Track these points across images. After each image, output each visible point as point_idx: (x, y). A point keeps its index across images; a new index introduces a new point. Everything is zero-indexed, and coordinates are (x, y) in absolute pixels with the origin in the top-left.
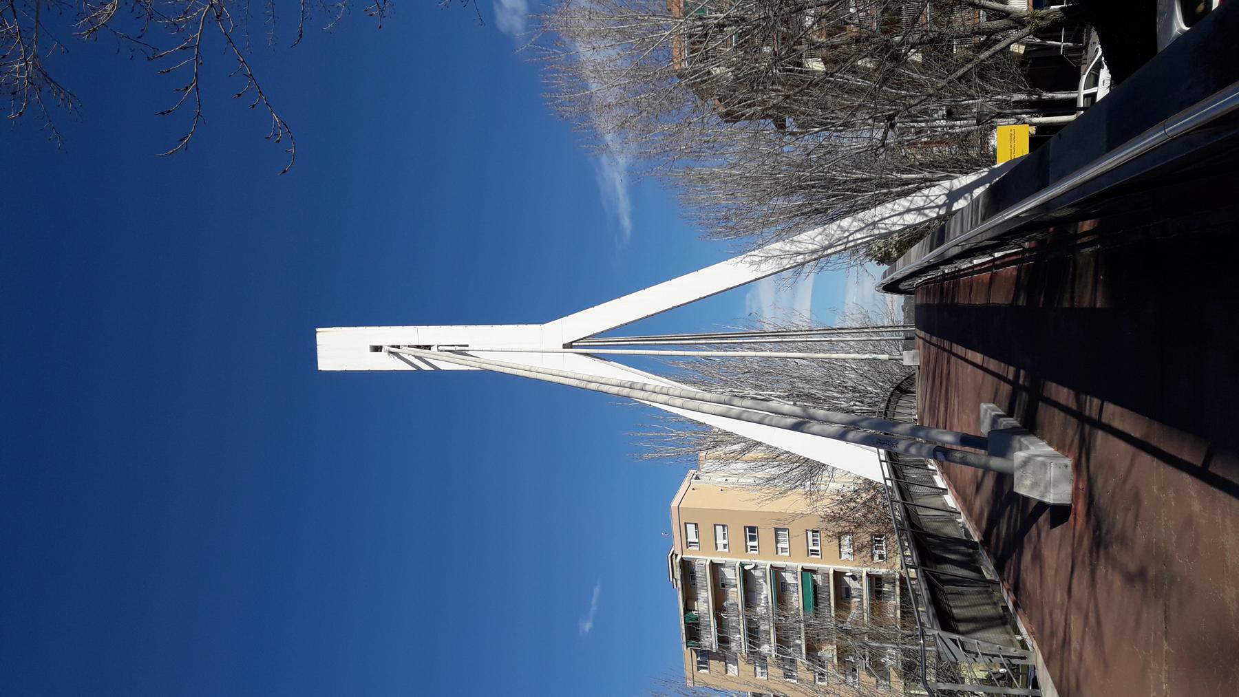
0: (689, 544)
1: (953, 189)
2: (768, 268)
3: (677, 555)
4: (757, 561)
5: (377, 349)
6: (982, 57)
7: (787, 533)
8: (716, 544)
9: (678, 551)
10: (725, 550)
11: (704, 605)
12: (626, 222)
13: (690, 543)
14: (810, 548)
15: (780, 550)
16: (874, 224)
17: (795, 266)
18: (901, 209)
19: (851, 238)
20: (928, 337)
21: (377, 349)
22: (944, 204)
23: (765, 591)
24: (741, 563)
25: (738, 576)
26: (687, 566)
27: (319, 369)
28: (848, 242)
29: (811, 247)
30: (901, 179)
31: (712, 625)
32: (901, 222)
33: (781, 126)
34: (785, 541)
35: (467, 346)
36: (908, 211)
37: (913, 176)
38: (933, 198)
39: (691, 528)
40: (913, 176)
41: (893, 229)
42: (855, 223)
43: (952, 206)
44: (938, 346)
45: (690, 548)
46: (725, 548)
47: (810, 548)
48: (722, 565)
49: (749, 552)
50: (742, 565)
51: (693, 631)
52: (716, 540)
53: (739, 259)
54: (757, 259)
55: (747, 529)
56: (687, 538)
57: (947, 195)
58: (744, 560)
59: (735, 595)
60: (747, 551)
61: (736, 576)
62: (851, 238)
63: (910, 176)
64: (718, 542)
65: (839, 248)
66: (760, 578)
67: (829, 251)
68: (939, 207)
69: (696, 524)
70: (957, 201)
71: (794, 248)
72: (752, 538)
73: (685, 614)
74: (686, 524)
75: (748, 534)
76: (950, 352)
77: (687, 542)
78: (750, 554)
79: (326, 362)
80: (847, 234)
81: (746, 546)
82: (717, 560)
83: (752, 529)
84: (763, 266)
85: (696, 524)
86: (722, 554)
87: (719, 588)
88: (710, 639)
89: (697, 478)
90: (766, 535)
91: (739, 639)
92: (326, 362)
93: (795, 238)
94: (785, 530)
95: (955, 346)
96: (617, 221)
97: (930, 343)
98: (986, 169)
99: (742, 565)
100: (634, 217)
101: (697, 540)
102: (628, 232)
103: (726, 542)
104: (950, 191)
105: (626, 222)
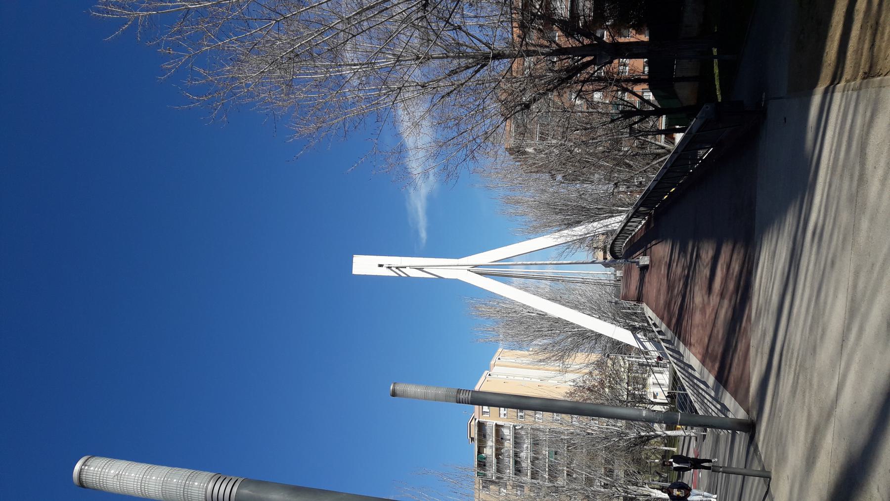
2: (561, 241)
3: (475, 419)
5: (381, 266)
6: (653, 163)
8: (500, 413)
9: (477, 417)
11: (489, 451)
12: (423, 235)
16: (607, 226)
17: (572, 241)
18: (618, 221)
19: (597, 231)
21: (381, 266)
25: (511, 433)
26: (481, 426)
27: (353, 273)
28: (596, 232)
29: (580, 233)
30: (618, 209)
31: (494, 462)
33: (553, 177)
37: (624, 209)
40: (624, 209)
41: (615, 228)
42: (599, 225)
45: (484, 415)
48: (502, 426)
51: (482, 464)
53: (549, 236)
54: (557, 236)
59: (508, 445)
61: (510, 433)
62: (597, 231)
63: (622, 209)
64: (501, 412)
65: (592, 235)
67: (588, 236)
71: (573, 233)
73: (478, 455)
79: (356, 271)
80: (595, 229)
82: (500, 423)
84: (559, 240)
87: (500, 439)
88: (491, 473)
89: (490, 375)
91: (510, 471)
92: (356, 271)
93: (573, 229)
96: (417, 232)
99: (514, 426)
100: (429, 231)
101: (488, 411)
102: (424, 241)
105: (423, 235)
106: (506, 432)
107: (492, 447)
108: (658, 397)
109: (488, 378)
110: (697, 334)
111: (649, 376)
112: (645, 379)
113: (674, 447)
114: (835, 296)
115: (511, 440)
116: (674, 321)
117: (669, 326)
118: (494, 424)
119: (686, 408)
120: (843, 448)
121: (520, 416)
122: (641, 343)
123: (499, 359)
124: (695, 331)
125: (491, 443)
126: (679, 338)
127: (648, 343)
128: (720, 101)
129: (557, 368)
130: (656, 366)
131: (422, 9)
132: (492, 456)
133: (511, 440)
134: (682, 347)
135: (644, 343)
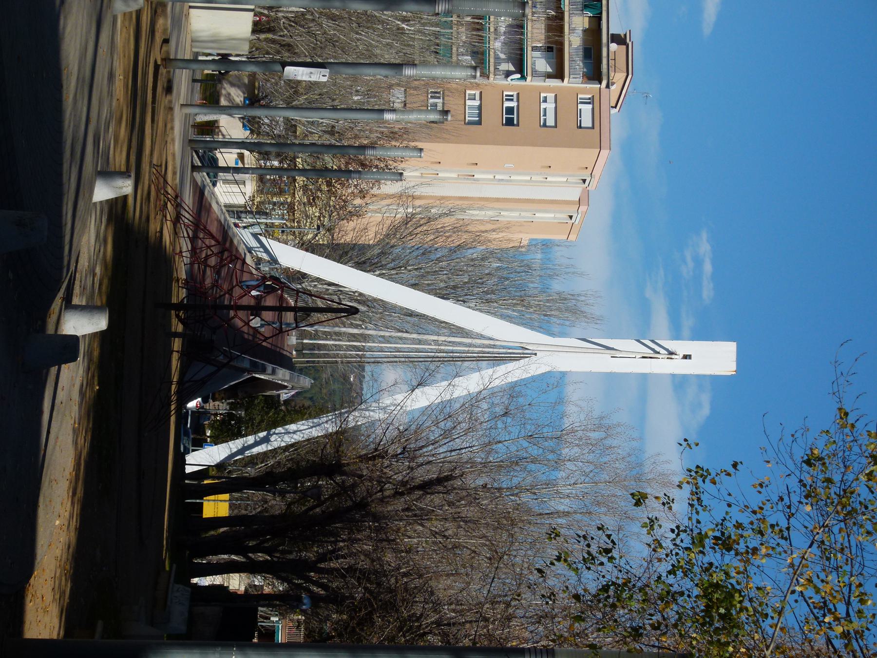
0: (591, 101)
1: (266, 444)
4: (505, 82)
5: (686, 357)
7: (467, 118)
10: (545, 95)
13: (589, 103)
14: (441, 101)
15: (477, 97)
20: (282, 351)
21: (686, 357)
22: (272, 435)
23: (497, 46)
24: (526, 80)
26: (594, 74)
32: (298, 426)
34: (471, 107)
35: (612, 357)
36: (295, 432)
38: (279, 439)
39: (587, 122)
43: (267, 434)
44: (277, 347)
45: (590, 96)
46: (546, 98)
47: (441, 101)
48: (549, 76)
49: (515, 93)
50: (523, 78)
52: (556, 108)
55: (515, 122)
56: (593, 109)
57: (270, 441)
58: (522, 83)
60: (518, 94)
66: (504, 61)
68: (274, 433)
69: (580, 127)
70: (264, 437)
72: (510, 110)
73: (601, 13)
74: (593, 127)
75: (515, 116)
76: (272, 345)
77: (593, 104)
78: (515, 91)
79: (730, 348)
81: (518, 101)
82: (555, 83)
83: (510, 122)
85: (580, 127)
86: (548, 90)
90: (493, 117)
92: (730, 348)
94: (471, 123)
95: (287, 427)
97: (280, 348)
98: (246, 455)
99: (523, 78)
103: (543, 106)
104: (268, 443)
106: (543, 65)
107: (572, 30)
108: (236, 156)
109: (586, 175)
111: (252, 199)
112: (260, 191)
113: (207, 74)
115: (530, 49)
118: (566, 80)
119: (209, 160)
121: (512, 100)
122: (262, 245)
123: (571, 217)
125: (573, 41)
126: (224, 228)
128: (200, 399)
129: (417, 203)
130: (241, 212)
132: (570, 14)
133: (530, 49)
135: (259, 246)
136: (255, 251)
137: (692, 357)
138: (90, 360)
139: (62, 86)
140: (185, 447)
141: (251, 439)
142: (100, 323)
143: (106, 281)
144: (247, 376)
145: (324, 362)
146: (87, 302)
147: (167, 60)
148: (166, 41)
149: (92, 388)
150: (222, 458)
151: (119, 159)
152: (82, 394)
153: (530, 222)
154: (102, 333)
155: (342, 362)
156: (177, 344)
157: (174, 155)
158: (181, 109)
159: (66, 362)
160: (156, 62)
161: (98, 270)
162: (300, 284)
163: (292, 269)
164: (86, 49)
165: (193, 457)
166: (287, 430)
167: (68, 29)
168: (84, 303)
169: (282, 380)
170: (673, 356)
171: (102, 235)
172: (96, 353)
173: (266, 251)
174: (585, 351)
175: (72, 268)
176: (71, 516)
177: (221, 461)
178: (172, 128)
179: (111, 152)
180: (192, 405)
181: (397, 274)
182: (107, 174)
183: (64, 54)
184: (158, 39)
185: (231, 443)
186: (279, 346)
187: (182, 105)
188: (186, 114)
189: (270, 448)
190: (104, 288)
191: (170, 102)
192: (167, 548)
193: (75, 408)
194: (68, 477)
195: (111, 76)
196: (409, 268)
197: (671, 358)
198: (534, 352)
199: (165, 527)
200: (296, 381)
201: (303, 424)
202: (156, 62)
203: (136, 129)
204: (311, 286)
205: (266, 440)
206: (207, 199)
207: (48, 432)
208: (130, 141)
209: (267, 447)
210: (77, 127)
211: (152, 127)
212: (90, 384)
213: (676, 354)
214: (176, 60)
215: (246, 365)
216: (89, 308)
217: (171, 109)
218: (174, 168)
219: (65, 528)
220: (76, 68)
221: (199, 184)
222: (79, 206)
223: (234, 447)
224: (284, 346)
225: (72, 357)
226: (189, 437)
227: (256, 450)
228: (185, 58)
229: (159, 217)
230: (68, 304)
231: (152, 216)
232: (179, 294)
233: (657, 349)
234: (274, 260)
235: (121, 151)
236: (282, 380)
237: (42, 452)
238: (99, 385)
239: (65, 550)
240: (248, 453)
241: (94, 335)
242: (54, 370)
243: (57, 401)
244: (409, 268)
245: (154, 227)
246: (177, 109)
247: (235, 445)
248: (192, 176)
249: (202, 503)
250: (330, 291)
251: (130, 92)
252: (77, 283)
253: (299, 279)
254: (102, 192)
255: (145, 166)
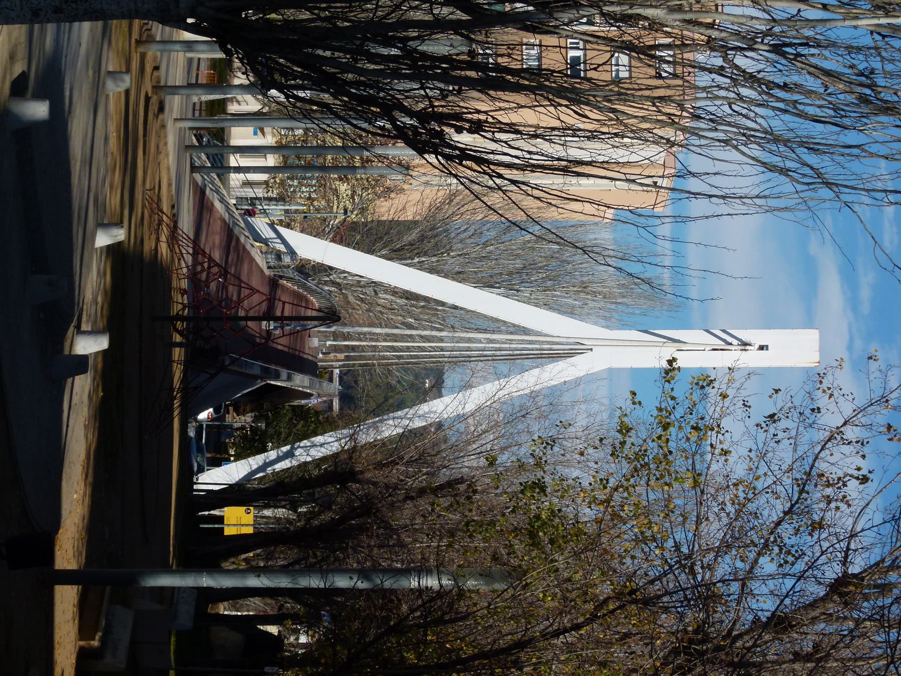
5: (761, 348)
20: (301, 355)
21: (761, 348)
22: (296, 449)
32: (326, 438)
36: (322, 445)
43: (291, 447)
68: (299, 447)
97: (300, 351)
110: (217, 226)
114: (167, 255)
116: (233, 243)
117: (238, 240)
120: (445, 416)
124: (218, 229)
126: (229, 226)
127: (268, 237)
128: (211, 410)
131: (840, 561)
134: (226, 216)
135: (275, 236)
136: (271, 242)
137: (769, 347)
138: (96, 371)
139: (71, 174)
140: (199, 465)
141: (272, 455)
142: (101, 343)
143: (106, 306)
144: (260, 384)
145: (360, 365)
146: (92, 328)
147: (157, 88)
148: (156, 68)
149: (97, 395)
150: (242, 475)
151: (114, 200)
152: (90, 398)
153: (607, 190)
154: (104, 352)
155: (379, 365)
156: (178, 353)
157: (168, 169)
158: (174, 124)
159: (78, 374)
160: (147, 94)
161: (100, 299)
162: (328, 276)
163: (314, 262)
164: (86, 134)
165: (209, 476)
166: (313, 443)
167: (74, 130)
168: (90, 329)
169: (303, 387)
170: (748, 347)
171: (102, 271)
172: (100, 366)
173: (284, 242)
174: (653, 345)
175: (81, 305)
176: (85, 494)
177: (240, 480)
178: (166, 144)
179: (108, 195)
180: (203, 416)
181: (438, 261)
182: (102, 225)
183: (71, 149)
184: (148, 69)
185: (251, 460)
186: (298, 348)
187: (176, 120)
188: (180, 129)
189: (295, 463)
190: (105, 311)
191: (163, 120)
192: (174, 554)
193: (86, 409)
194: (82, 463)
195: (106, 139)
196: (452, 254)
197: (745, 350)
198: (590, 347)
199: (172, 534)
200: (317, 387)
201: (330, 436)
202: (147, 94)
203: (129, 168)
204: (340, 278)
205: (290, 455)
206: (208, 198)
207: (68, 426)
208: (123, 183)
209: (291, 462)
210: (81, 198)
211: (144, 159)
212: (96, 390)
213: (750, 345)
214: (166, 86)
215: (257, 371)
216: (94, 332)
217: (163, 126)
218: (169, 179)
219: (81, 502)
220: (80, 154)
221: (200, 184)
222: (84, 257)
223: (254, 463)
224: (304, 348)
225: (84, 371)
226: (203, 454)
227: (279, 467)
228: (177, 84)
229: (154, 237)
230: (79, 330)
231: (146, 238)
232: (179, 303)
233: (729, 339)
234: (292, 252)
235: (116, 195)
236: (303, 387)
237: (64, 440)
238: (103, 391)
239: (81, 520)
240: (269, 470)
241: (97, 353)
242: (70, 380)
243: (73, 403)
244: (452, 254)
245: (149, 246)
246: (170, 125)
247: (255, 461)
248: (191, 177)
249: (223, 528)
250: (362, 283)
251: (122, 141)
252: (84, 313)
253: (326, 270)
254: (103, 240)
255: (139, 196)
